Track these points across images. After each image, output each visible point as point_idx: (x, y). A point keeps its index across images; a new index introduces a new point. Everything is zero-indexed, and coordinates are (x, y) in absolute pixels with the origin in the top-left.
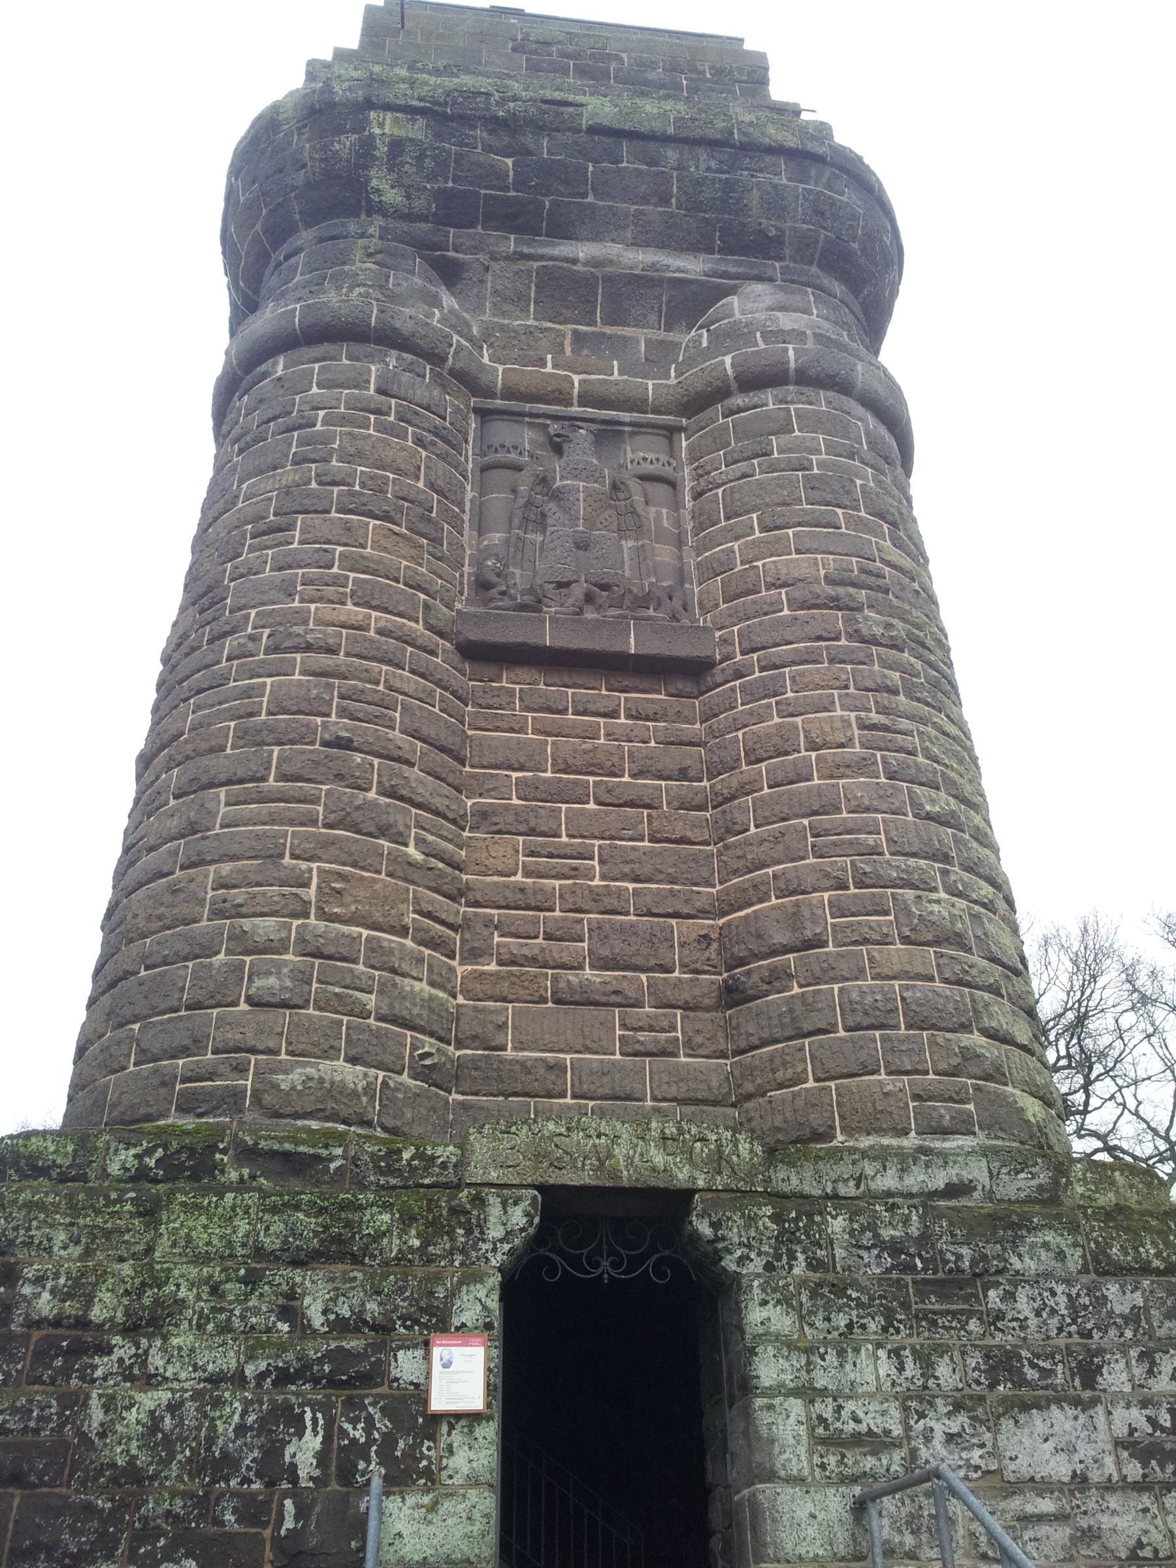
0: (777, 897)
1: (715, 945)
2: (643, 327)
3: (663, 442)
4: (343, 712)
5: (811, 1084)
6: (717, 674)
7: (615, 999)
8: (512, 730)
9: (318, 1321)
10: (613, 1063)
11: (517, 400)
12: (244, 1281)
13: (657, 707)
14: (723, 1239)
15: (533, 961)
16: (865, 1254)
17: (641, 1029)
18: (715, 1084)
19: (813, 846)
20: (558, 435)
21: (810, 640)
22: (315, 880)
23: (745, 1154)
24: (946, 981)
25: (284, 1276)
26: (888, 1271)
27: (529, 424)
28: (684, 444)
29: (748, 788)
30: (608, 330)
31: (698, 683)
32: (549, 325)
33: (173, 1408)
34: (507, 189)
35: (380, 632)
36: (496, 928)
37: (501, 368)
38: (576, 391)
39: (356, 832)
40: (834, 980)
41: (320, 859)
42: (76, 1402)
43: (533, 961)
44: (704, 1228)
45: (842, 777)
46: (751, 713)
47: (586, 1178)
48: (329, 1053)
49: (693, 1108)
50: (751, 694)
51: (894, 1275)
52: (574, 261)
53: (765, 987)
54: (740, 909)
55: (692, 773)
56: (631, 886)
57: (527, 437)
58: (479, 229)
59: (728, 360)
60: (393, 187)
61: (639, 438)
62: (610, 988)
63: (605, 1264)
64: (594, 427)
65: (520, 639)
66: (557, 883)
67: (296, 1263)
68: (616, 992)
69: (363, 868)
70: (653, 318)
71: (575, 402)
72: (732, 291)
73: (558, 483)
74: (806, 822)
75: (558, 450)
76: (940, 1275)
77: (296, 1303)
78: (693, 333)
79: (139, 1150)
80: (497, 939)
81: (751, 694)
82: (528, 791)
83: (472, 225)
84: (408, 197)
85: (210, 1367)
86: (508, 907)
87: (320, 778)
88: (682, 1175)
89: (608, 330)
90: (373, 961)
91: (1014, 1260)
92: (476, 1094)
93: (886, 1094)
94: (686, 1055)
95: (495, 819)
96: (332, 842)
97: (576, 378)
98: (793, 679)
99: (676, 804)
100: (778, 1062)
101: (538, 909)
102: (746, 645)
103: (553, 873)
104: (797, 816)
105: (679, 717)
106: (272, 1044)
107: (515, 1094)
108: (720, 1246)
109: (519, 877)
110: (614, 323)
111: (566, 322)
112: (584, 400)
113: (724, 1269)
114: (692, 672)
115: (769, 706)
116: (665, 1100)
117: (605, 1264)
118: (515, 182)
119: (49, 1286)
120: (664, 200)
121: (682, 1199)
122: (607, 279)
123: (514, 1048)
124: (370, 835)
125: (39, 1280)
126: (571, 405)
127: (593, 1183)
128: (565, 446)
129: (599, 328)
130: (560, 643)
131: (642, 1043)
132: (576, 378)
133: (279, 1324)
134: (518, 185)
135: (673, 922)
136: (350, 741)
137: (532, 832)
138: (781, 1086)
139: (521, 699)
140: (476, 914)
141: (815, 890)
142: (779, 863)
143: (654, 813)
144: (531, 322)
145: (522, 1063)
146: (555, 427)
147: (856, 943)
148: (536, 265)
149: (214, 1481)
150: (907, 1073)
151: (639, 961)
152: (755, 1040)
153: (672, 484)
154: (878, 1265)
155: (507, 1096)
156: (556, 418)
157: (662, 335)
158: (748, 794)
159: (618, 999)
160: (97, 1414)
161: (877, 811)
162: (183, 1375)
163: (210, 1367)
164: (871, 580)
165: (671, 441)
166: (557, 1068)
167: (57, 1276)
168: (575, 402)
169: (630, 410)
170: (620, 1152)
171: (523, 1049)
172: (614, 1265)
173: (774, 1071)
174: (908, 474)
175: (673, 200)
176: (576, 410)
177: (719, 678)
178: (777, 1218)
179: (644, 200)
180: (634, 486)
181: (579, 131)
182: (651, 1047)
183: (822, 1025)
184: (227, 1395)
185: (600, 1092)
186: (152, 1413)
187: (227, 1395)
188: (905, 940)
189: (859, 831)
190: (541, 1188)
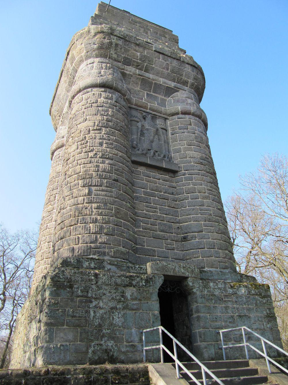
0: (193, 222)
1: (180, 229)
2: (160, 95)
3: (163, 121)
4: (115, 173)
5: (200, 258)
6: (179, 174)
7: (163, 238)
8: (141, 180)
9: (129, 297)
10: (163, 251)
11: (137, 106)
12: (115, 289)
13: (167, 179)
14: (194, 286)
15: (149, 229)
16: (216, 290)
17: (168, 245)
18: (181, 256)
19: (200, 212)
20: (145, 116)
21: (197, 170)
22: (114, 209)
23: (197, 271)
24: (223, 241)
25: (121, 289)
26: (219, 293)
27: (139, 112)
28: (168, 122)
29: (187, 198)
30: (153, 94)
31: (174, 175)
32: (142, 90)
33: (105, 313)
34: (138, 60)
35: (120, 157)
36: (141, 221)
37: (134, 99)
38: (149, 107)
39: (120, 200)
40: (204, 239)
41: (114, 205)
42: (87, 312)
43: (149, 229)
44: (191, 284)
45: (204, 199)
46: (187, 183)
47: (172, 274)
48: (120, 245)
49: (178, 261)
50: (186, 179)
51: (220, 294)
52: (149, 78)
53: (191, 239)
54: (185, 223)
55: (174, 194)
56: (165, 216)
57: (139, 115)
58: (131, 67)
59: (179, 107)
60: (115, 54)
61: (159, 119)
62: (162, 236)
63: (169, 289)
64: (152, 115)
65: (143, 161)
66: (152, 213)
67: (124, 287)
68: (164, 237)
69: (121, 208)
70: (162, 93)
71: (148, 109)
72: (177, 91)
73: (147, 127)
74: (198, 207)
75: (144, 119)
76: (227, 294)
77: (124, 294)
78: (169, 98)
79: (89, 262)
80: (142, 224)
81: (186, 179)
82: (146, 193)
83: (130, 66)
84: (118, 57)
85: (111, 306)
86: (143, 218)
87: (113, 187)
88: (187, 274)
89: (153, 94)
90: (125, 227)
91: (238, 292)
92: (140, 255)
93: (214, 261)
94: (176, 250)
95: (140, 199)
96: (115, 202)
97: (149, 104)
98: (195, 178)
99: (172, 200)
100: (194, 253)
101: (149, 219)
102: (185, 169)
103: (151, 211)
104: (197, 206)
105: (171, 182)
106: (110, 243)
107: (147, 255)
108: (193, 287)
109: (145, 212)
110: (155, 93)
111: (146, 91)
112: (150, 109)
113: (193, 291)
114: (174, 172)
115: (190, 183)
116: (173, 258)
117: (169, 289)
118: (140, 59)
119: (80, 289)
120: (168, 69)
121: (186, 278)
122: (155, 84)
123: (146, 246)
124: (122, 201)
125: (78, 288)
126: (148, 109)
127: (173, 275)
128: (146, 118)
129: (152, 93)
130: (151, 163)
131: (169, 247)
132: (149, 104)
133: (122, 298)
134: (140, 59)
135: (172, 224)
136: (118, 180)
137: (147, 202)
138: (195, 258)
139: (142, 174)
140: (138, 218)
141: (201, 221)
142: (193, 215)
143: (168, 201)
144: (139, 89)
145: (148, 249)
146: (144, 114)
147: (208, 232)
148: (142, 77)
149: (114, 327)
150: (217, 257)
151: (167, 231)
152: (189, 249)
153: (166, 130)
154: (218, 292)
155: (146, 256)
156: (144, 112)
157: (163, 97)
158: (186, 200)
159: (164, 238)
160: (92, 313)
161: (211, 207)
162: (106, 307)
163: (111, 306)
164: (207, 159)
165: (165, 121)
166: (154, 251)
167: (81, 287)
168: (148, 109)
169: (159, 113)
170: (177, 269)
171: (148, 247)
172: (170, 289)
173: (193, 255)
174: (207, 134)
175: (169, 70)
176: (148, 111)
177: (179, 175)
178: (202, 283)
179: (164, 68)
180: (160, 130)
181: (152, 50)
182: (170, 248)
183: (202, 247)
184: (115, 311)
185: (162, 256)
186: (102, 314)
187: (115, 311)
188: (217, 233)
189: (208, 211)
190: (164, 275)
